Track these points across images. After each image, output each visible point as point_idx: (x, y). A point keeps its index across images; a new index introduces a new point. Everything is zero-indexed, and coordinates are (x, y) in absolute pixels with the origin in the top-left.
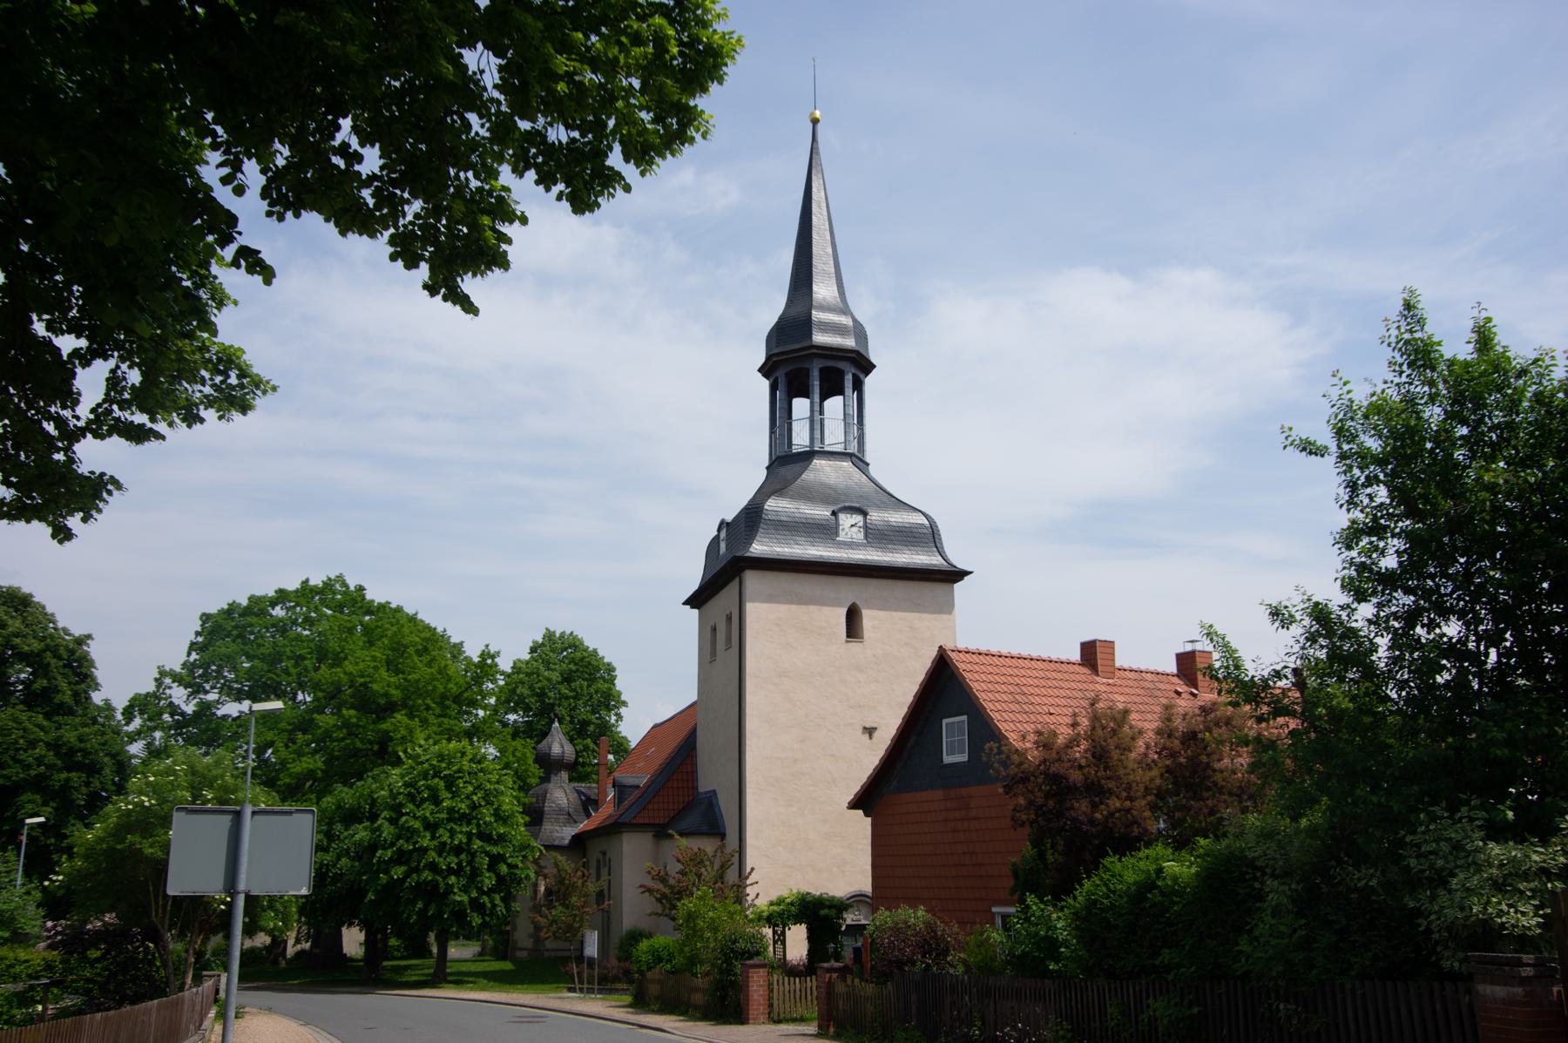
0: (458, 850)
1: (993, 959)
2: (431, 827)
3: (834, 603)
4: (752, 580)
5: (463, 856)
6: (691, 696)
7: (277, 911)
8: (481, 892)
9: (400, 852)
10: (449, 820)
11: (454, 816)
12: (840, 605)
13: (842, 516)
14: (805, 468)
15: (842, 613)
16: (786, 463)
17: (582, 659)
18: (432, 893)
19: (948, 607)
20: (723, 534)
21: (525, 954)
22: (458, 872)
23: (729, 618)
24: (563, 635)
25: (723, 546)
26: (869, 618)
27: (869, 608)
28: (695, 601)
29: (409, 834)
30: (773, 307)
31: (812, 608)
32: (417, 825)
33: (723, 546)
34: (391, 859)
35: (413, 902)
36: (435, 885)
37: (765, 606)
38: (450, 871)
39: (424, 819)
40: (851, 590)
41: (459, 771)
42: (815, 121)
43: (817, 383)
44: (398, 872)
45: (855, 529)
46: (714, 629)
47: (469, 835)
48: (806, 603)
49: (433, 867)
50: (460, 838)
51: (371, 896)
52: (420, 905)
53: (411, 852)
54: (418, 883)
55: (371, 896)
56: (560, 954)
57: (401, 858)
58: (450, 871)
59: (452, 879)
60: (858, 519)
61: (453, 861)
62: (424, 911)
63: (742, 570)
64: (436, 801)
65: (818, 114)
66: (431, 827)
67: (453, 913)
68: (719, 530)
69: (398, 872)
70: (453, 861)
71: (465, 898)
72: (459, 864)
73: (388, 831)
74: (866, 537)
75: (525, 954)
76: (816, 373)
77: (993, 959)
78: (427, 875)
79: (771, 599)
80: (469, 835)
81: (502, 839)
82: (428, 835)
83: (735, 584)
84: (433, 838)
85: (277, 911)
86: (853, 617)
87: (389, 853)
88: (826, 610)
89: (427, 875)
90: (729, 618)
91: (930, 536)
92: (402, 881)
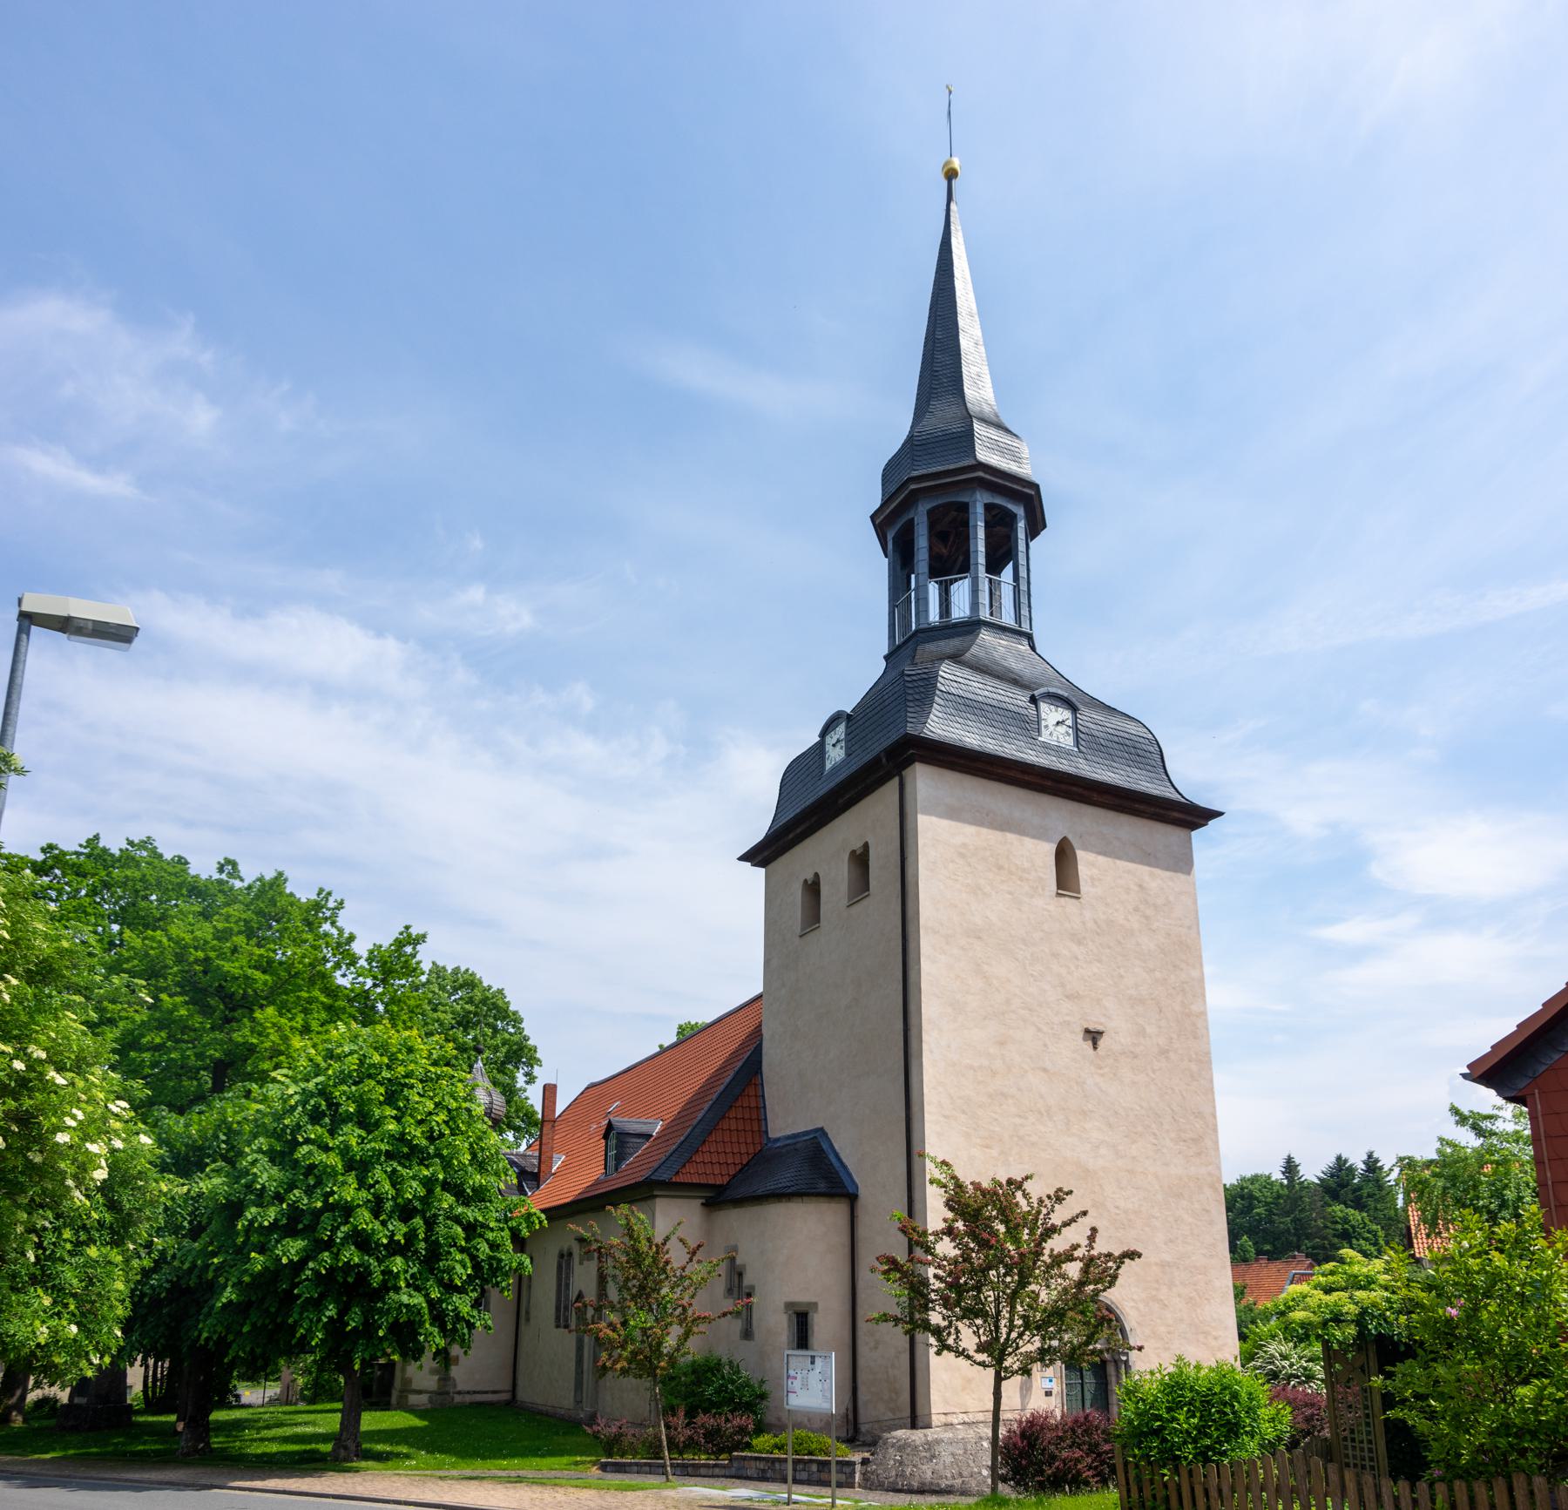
0: (406, 1213)
1: (289, 1363)
2: (359, 1167)
3: (1040, 834)
4: (924, 781)
5: (418, 1221)
6: (758, 988)
7: (58, 1291)
8: (450, 1288)
9: (295, 1213)
10: (390, 1155)
11: (404, 1151)
12: (1048, 840)
13: (1043, 706)
14: (973, 642)
15: (1048, 850)
16: (916, 651)
17: (484, 1001)
18: (355, 1288)
19: (1182, 863)
20: (840, 732)
21: (424, 1398)
22: (403, 1249)
23: (861, 859)
24: (456, 971)
25: (835, 755)
26: (1088, 863)
27: (1085, 849)
28: (759, 855)
29: (315, 1176)
30: (892, 422)
31: (1010, 836)
32: (333, 1160)
33: (835, 755)
34: (274, 1226)
35: (317, 1304)
36: (363, 1275)
37: (945, 823)
38: (394, 1248)
39: (345, 1151)
40: (1064, 817)
41: (408, 1075)
42: (951, 175)
43: (981, 524)
44: (292, 1248)
45: (1062, 729)
46: (813, 889)
47: (429, 1183)
48: (1002, 830)
49: (362, 1241)
50: (413, 1189)
51: (229, 1295)
52: (331, 1311)
53: (317, 1214)
54: (332, 1270)
55: (229, 1295)
56: (479, 1398)
57: (293, 1224)
58: (394, 1248)
59: (398, 1263)
60: (1066, 714)
61: (400, 1230)
62: (335, 1326)
63: (909, 762)
64: (366, 1122)
65: (956, 163)
66: (359, 1167)
67: (395, 1328)
68: (825, 732)
69: (292, 1248)
70: (400, 1230)
71: (418, 1300)
72: (411, 1236)
73: (267, 1175)
74: (1077, 744)
75: (424, 1398)
76: (980, 510)
77: (289, 1363)
78: (351, 1255)
79: (953, 814)
80: (429, 1183)
81: (481, 1196)
82: (351, 1179)
83: (890, 789)
84: (362, 1184)
85: (58, 1291)
86: (1064, 856)
87: (272, 1213)
88: (1029, 842)
89: (351, 1255)
90: (861, 859)
91: (1149, 754)
92: (297, 1267)
